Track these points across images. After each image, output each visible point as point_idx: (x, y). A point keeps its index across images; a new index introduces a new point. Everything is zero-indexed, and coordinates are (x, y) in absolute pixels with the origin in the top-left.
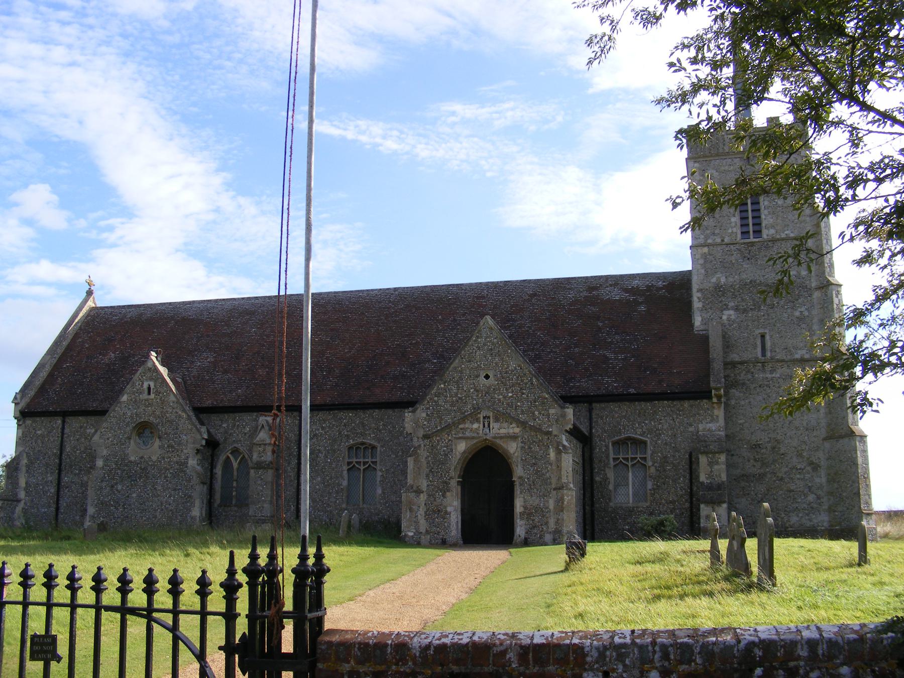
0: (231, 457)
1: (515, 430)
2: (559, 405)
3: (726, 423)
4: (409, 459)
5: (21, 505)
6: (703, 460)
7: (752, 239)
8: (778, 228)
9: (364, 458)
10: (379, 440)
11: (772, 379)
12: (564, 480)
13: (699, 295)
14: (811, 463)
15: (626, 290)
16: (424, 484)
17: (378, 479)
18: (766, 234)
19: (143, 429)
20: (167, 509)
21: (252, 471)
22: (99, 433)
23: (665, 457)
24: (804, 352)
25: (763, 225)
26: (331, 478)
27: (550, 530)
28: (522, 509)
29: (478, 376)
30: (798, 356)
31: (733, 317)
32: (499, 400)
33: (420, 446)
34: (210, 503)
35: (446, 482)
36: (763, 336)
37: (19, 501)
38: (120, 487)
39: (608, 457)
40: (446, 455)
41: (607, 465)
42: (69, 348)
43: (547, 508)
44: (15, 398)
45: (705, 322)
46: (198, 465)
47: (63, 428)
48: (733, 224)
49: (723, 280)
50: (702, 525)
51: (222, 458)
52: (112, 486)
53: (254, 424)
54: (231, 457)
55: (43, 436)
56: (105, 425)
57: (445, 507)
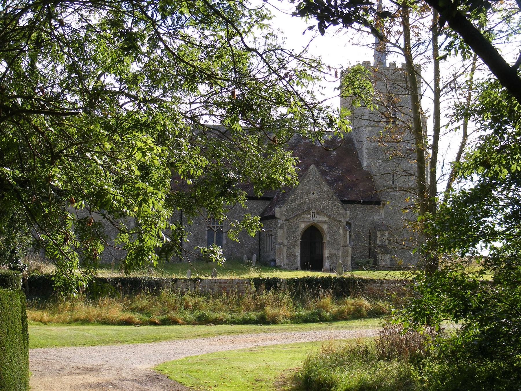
13: (366, 151)
16: (286, 242)
26: (199, 235)
29: (310, 193)
35: (295, 242)
40: (296, 229)
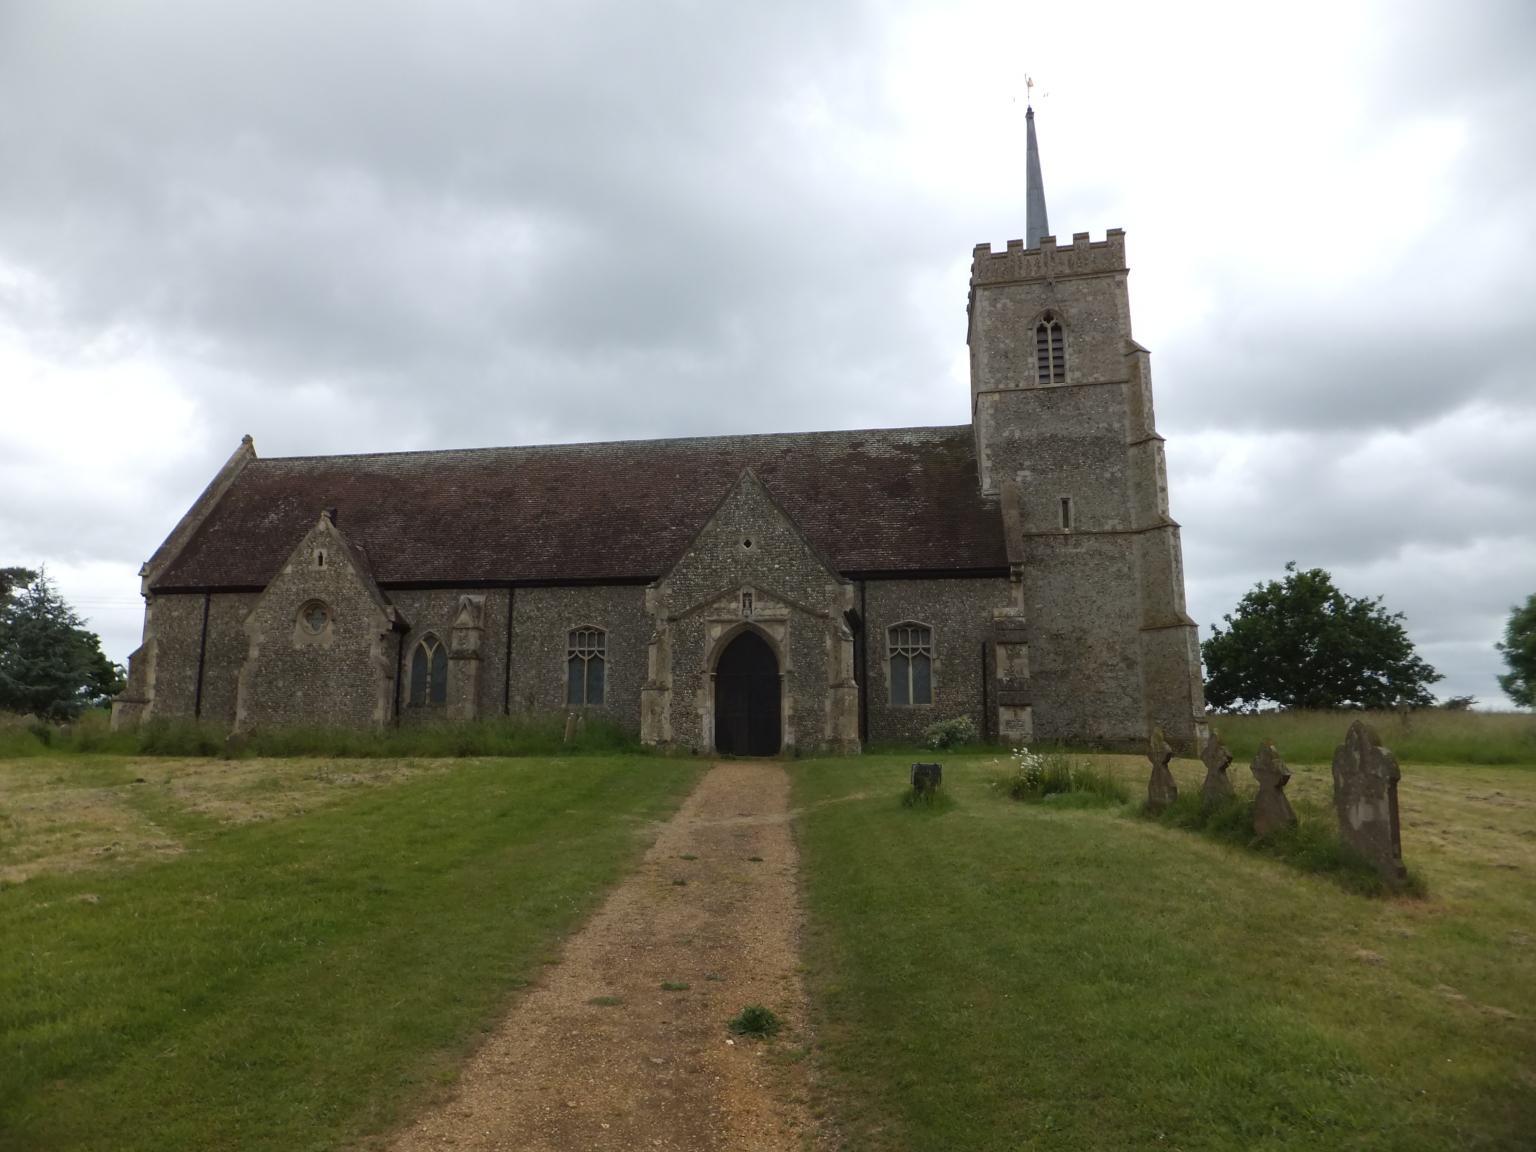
0: (424, 644)
1: (783, 611)
2: (837, 581)
3: (1026, 604)
4: (651, 648)
5: (150, 706)
6: (1001, 652)
7: (1053, 384)
8: (1085, 370)
9: (589, 646)
10: (607, 624)
11: (1077, 554)
12: (844, 675)
13: (989, 452)
14: (1125, 659)
15: (897, 447)
17: (606, 672)
18: (1069, 380)
19: (314, 609)
20: (341, 710)
21: (451, 663)
22: (254, 613)
23: (954, 648)
24: (1116, 521)
25: (1067, 366)
26: (548, 672)
27: (827, 738)
28: (791, 712)
29: (736, 543)
30: (1108, 527)
31: (1029, 479)
32: (763, 573)
33: (664, 630)
34: (397, 702)
36: (1065, 502)
37: (146, 702)
38: (281, 684)
39: (883, 646)
40: (697, 642)
41: (882, 657)
42: (218, 508)
43: (823, 710)
44: (143, 569)
45: (994, 485)
46: (383, 654)
47: (207, 609)
48: (1031, 366)
49: (1017, 435)
50: (1001, 733)
51: (414, 646)
52: (271, 683)
53: (453, 603)
54: (424, 644)
55: (180, 619)
56: (262, 604)
57: (696, 709)
